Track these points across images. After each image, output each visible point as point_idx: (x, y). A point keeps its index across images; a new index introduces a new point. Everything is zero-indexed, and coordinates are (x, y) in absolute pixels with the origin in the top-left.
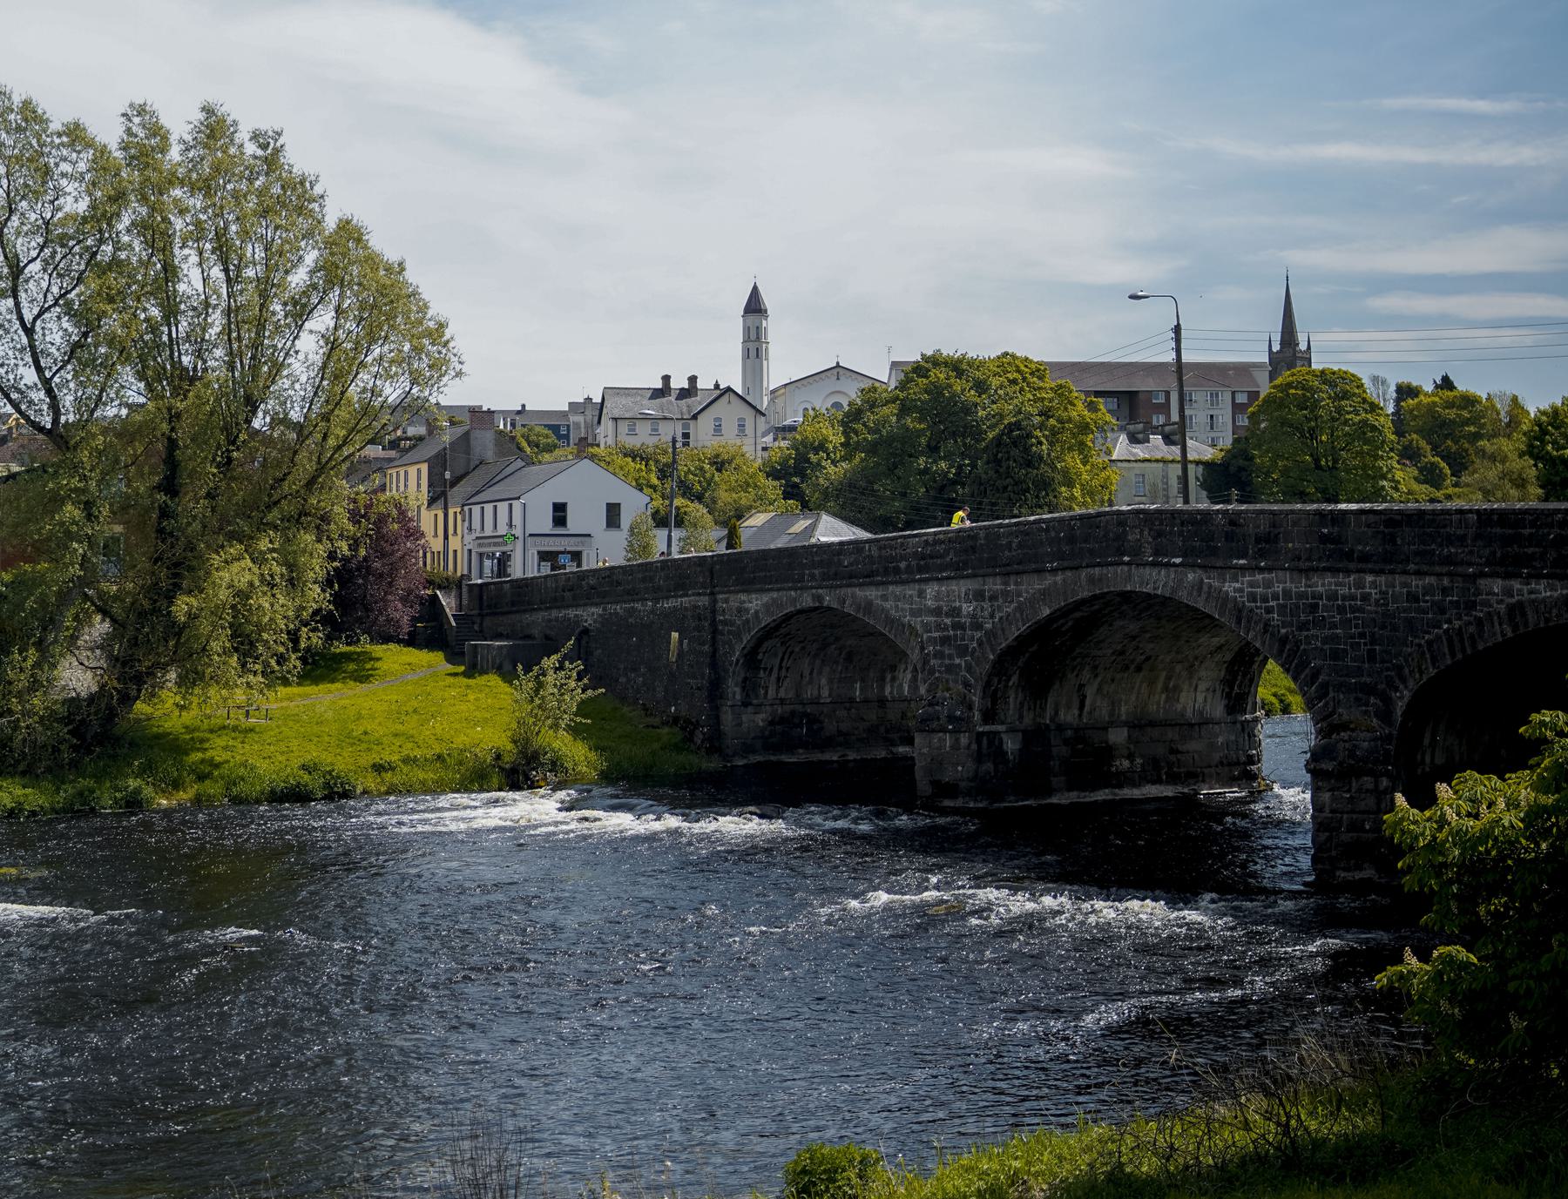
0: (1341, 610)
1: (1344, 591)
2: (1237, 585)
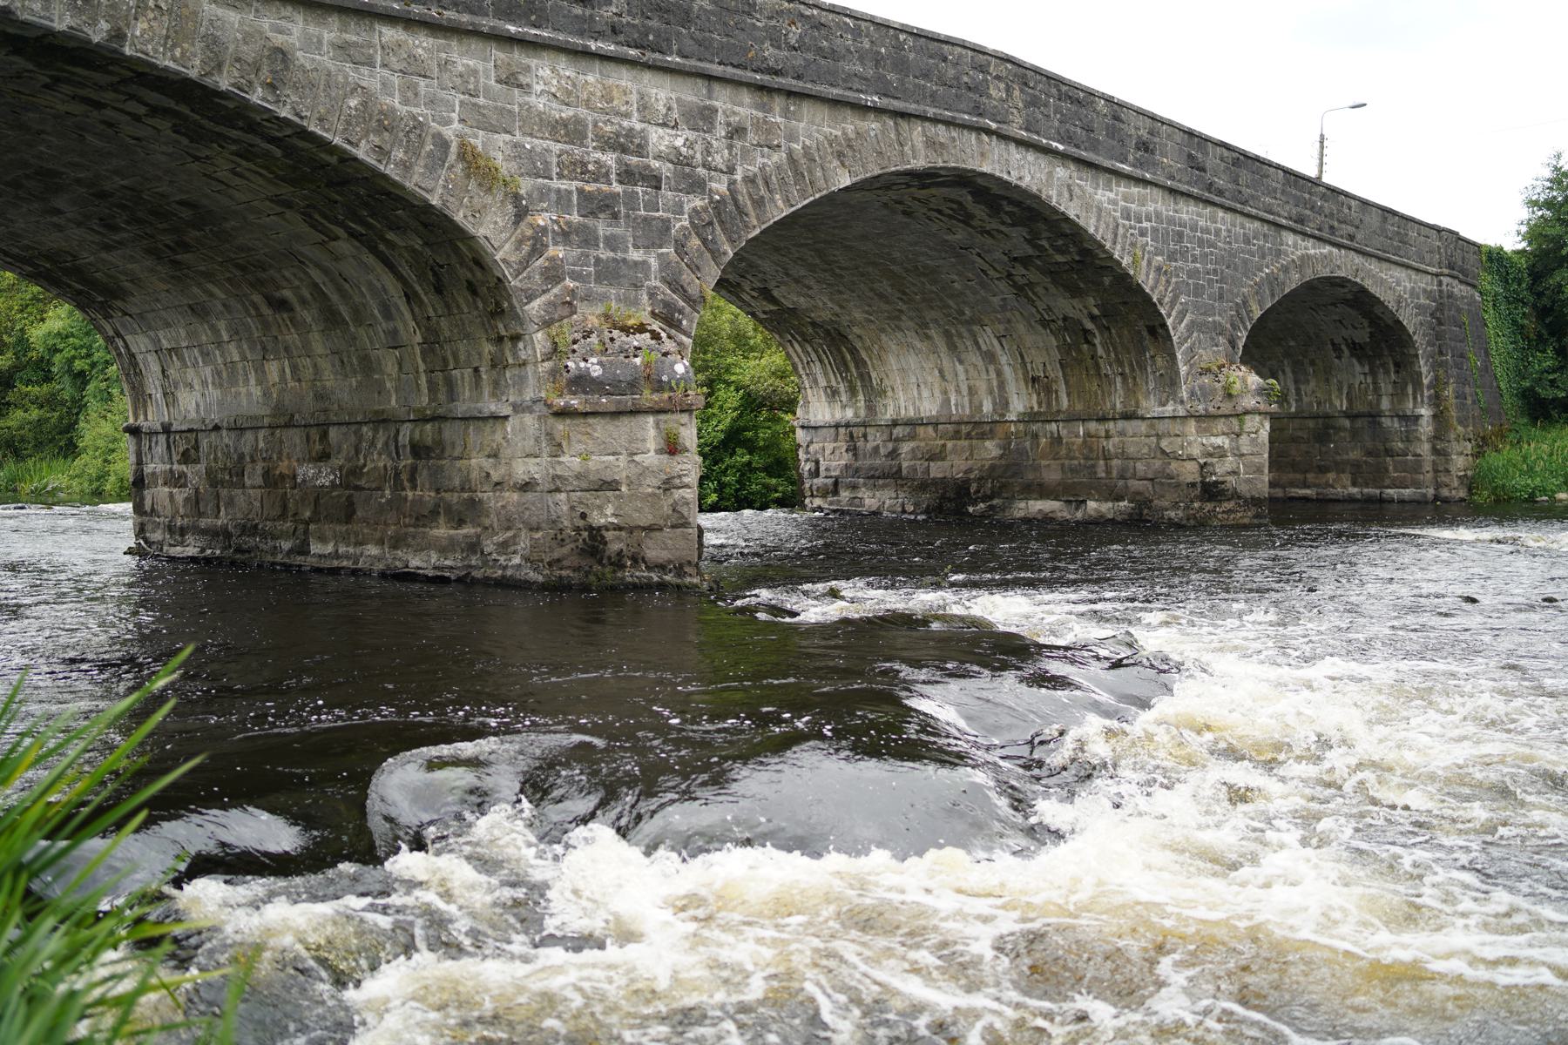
0: (1201, 243)
1: (1202, 223)
2: (1112, 195)
